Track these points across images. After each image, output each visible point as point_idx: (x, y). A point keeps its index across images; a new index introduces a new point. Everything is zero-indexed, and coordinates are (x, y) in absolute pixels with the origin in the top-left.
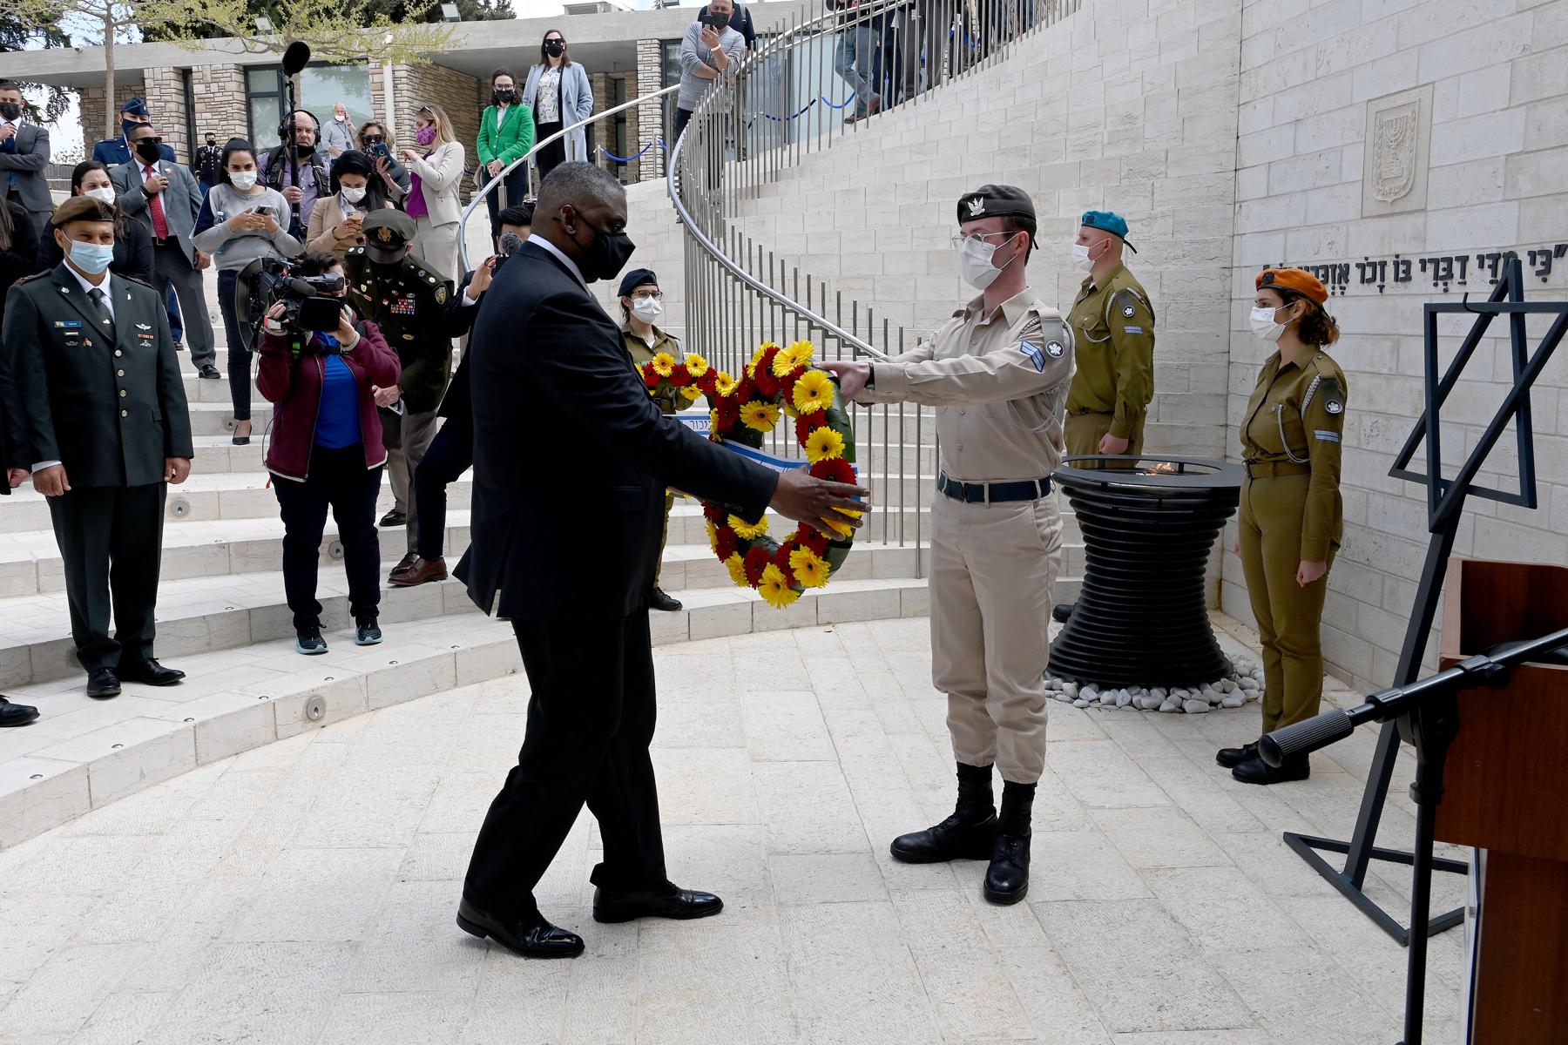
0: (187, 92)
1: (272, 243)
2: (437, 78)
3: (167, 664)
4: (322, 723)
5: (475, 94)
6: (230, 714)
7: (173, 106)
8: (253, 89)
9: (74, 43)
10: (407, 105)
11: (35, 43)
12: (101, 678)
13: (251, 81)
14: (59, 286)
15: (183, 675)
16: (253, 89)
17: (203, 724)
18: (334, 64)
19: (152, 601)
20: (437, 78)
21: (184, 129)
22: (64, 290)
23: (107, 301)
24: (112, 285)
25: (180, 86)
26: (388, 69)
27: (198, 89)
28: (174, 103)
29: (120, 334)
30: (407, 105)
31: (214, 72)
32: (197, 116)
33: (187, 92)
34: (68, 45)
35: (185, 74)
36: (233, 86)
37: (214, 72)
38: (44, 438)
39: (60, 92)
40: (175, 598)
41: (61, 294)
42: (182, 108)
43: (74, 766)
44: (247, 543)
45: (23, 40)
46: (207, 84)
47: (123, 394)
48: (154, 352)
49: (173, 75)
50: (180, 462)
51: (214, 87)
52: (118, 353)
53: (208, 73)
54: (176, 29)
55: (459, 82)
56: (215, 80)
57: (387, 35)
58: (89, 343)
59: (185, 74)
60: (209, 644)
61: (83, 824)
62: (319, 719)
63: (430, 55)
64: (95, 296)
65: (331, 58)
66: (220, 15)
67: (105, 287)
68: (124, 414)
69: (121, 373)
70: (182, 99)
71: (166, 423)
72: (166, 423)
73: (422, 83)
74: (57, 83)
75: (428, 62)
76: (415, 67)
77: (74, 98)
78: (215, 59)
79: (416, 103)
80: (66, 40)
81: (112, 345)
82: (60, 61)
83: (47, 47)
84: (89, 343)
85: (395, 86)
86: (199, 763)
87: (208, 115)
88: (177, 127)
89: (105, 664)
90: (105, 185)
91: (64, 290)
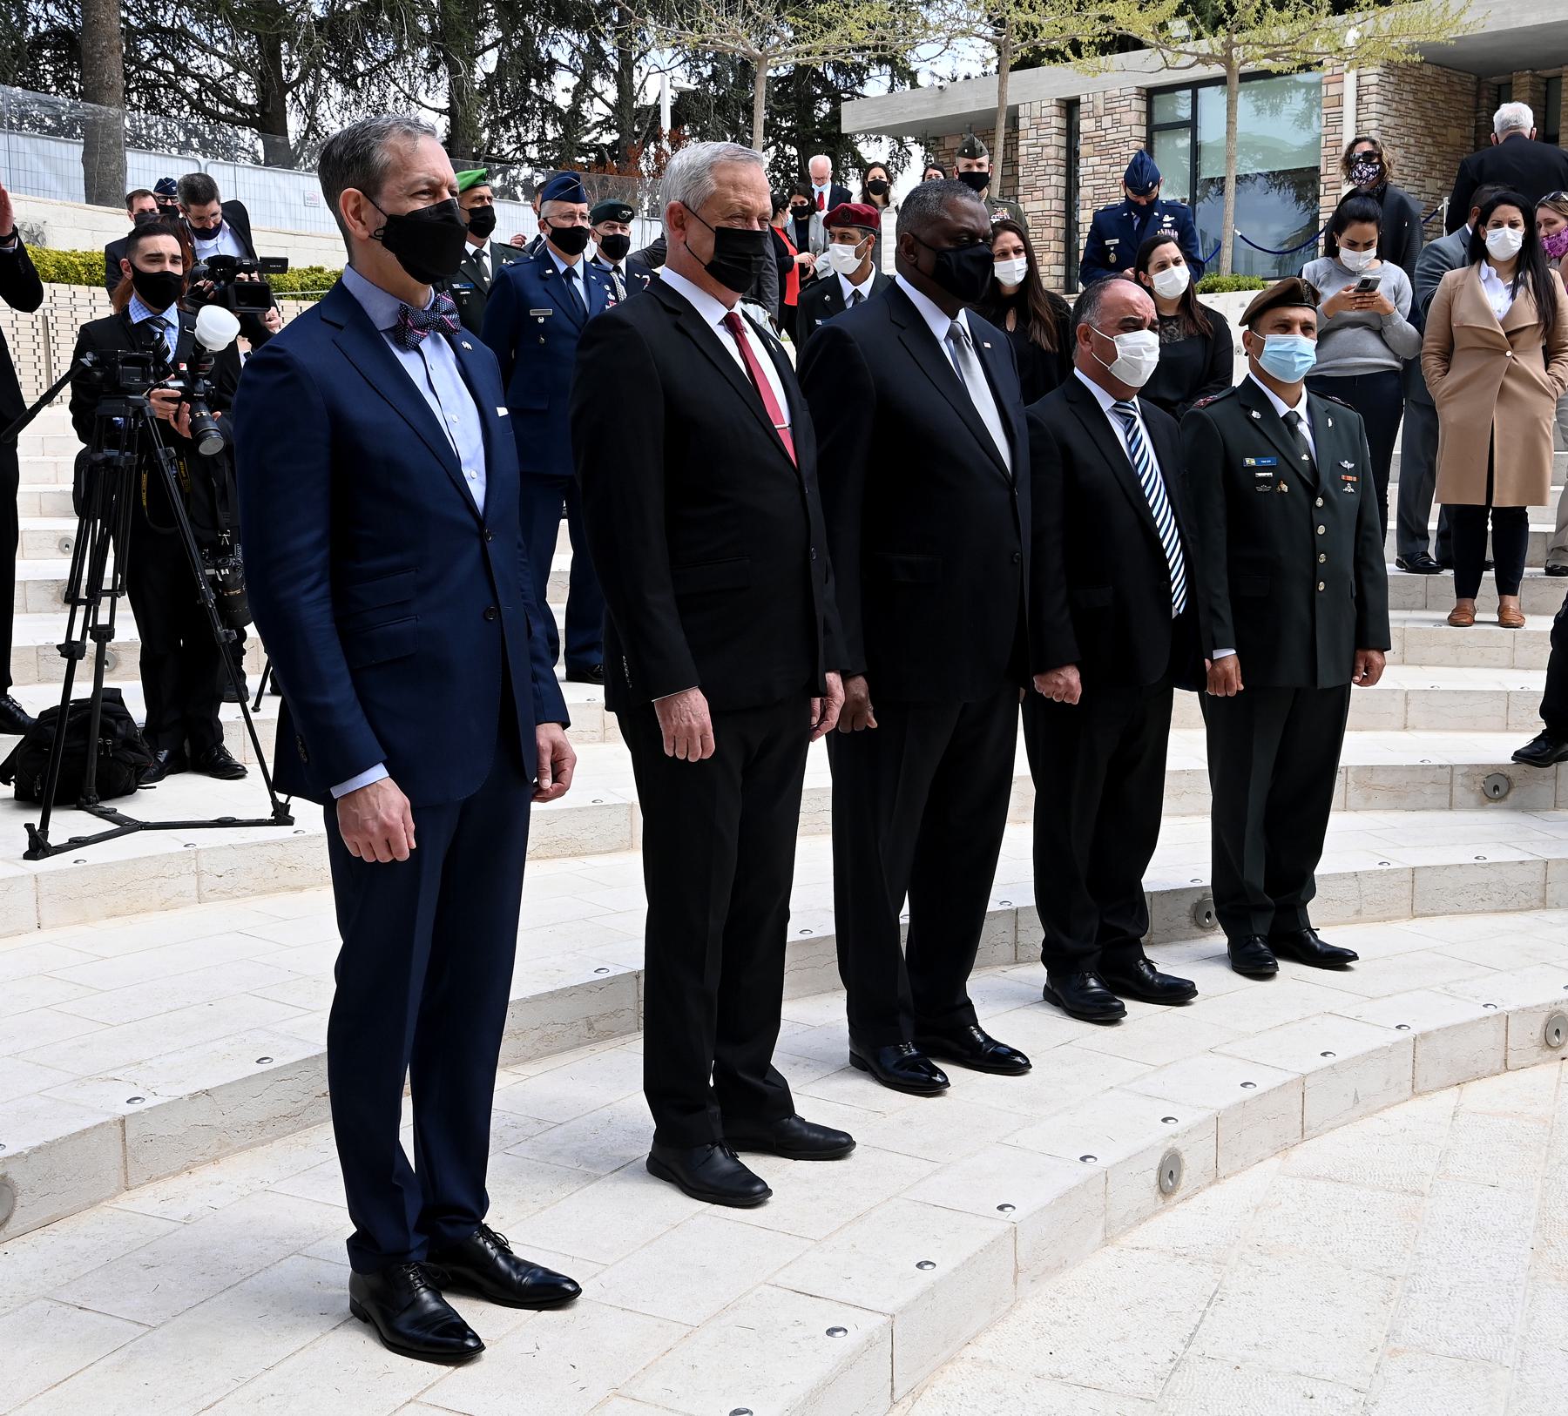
0: (1071, 132)
1: (1379, 333)
2: (1420, 80)
3: (1329, 936)
4: (1562, 1053)
5: (1471, 100)
6: (1456, 1026)
7: (1051, 151)
8: (1159, 119)
9: (923, 79)
10: (1374, 124)
11: (877, 83)
12: (1250, 948)
13: (1156, 108)
14: (1249, 409)
15: (1355, 957)
16: (1159, 119)
17: (1425, 1036)
18: (1280, 74)
19: (1314, 850)
20: (1420, 80)
21: (1062, 181)
22: (1255, 414)
23: (1304, 428)
24: (1309, 407)
25: (1062, 123)
26: (1350, 79)
27: (1086, 125)
28: (1053, 147)
29: (1324, 476)
30: (1374, 124)
31: (1107, 100)
32: (1082, 162)
33: (1071, 132)
34: (914, 85)
35: (1070, 107)
36: (1132, 117)
37: (1107, 100)
38: (1219, 617)
39: (901, 144)
40: (1352, 842)
41: (1251, 419)
42: (1063, 153)
43: (1289, 1077)
44: (1372, 768)
45: (862, 83)
46: (1098, 119)
47: (1322, 558)
48: (1356, 499)
49: (1055, 110)
50: (1374, 655)
51: (1107, 122)
52: (1320, 502)
53: (1100, 103)
54: (1076, 47)
55: (1450, 83)
56: (1109, 112)
57: (1352, 30)
58: (1285, 488)
59: (1070, 107)
60: (1358, 912)
61: (1302, 1156)
62: (1560, 1046)
63: (1423, 48)
64: (1290, 421)
65: (1274, 67)
66: (1139, 24)
67: (1301, 409)
68: (1322, 586)
69: (1321, 530)
70: (1062, 141)
71: (1361, 602)
72: (1361, 602)
73: (1398, 88)
74: (898, 134)
75: (1417, 58)
76: (1390, 66)
77: (917, 151)
78: (1111, 84)
79: (1387, 121)
80: (913, 76)
81: (1313, 489)
82: (914, 106)
83: (891, 90)
84: (1285, 488)
85: (1359, 98)
86: (1416, 1093)
87: (1097, 160)
88: (1054, 178)
89: (1256, 931)
90: (1176, 262)
91: (1255, 414)
